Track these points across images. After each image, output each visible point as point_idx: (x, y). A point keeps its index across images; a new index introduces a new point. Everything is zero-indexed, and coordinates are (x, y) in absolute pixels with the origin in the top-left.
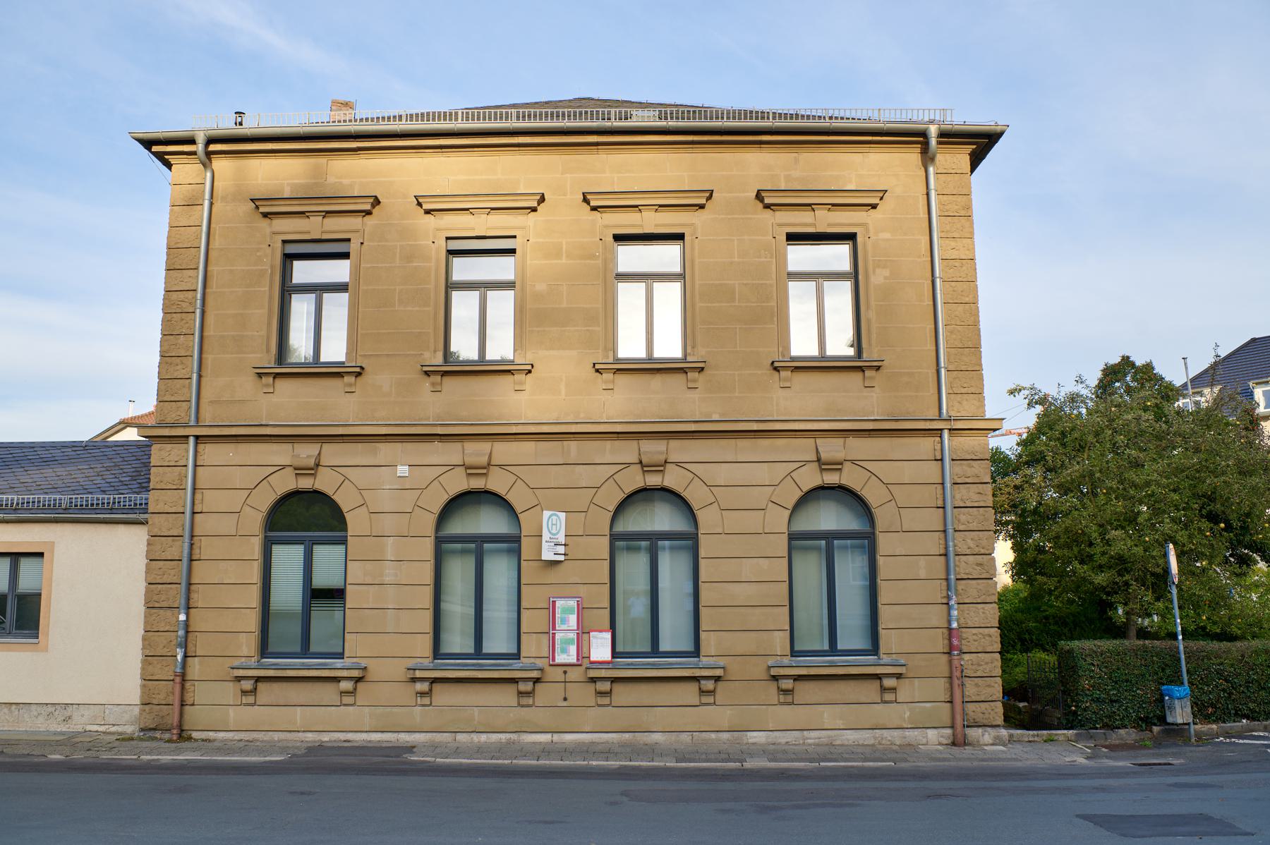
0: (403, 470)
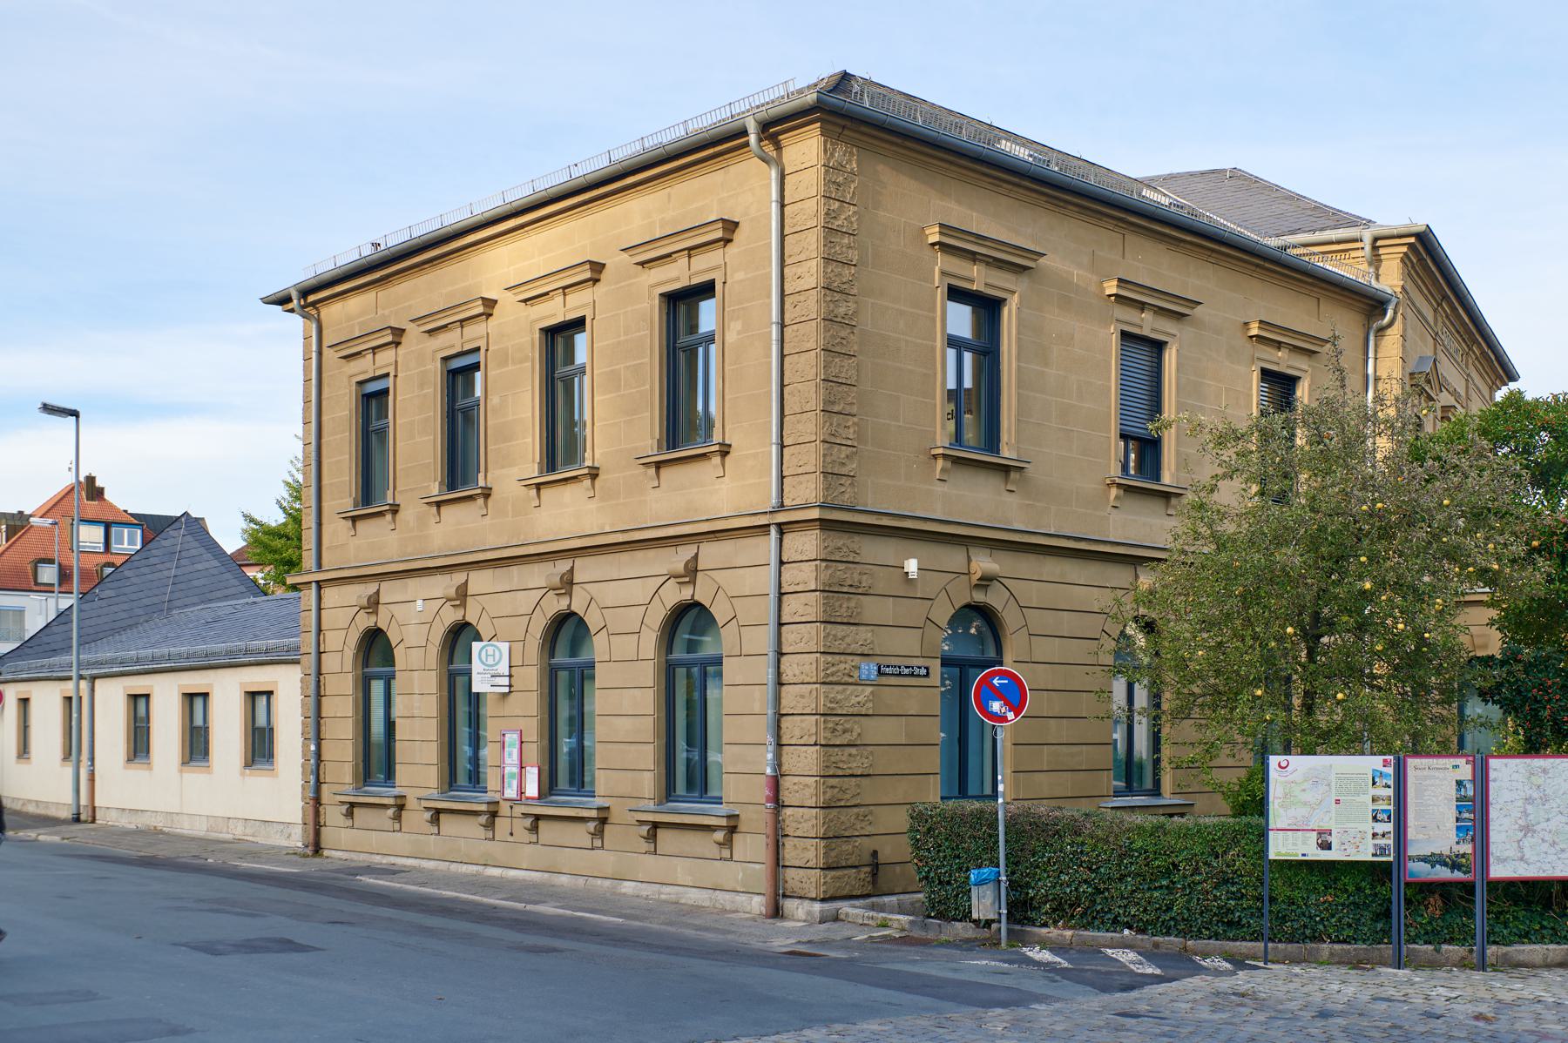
0: (419, 602)
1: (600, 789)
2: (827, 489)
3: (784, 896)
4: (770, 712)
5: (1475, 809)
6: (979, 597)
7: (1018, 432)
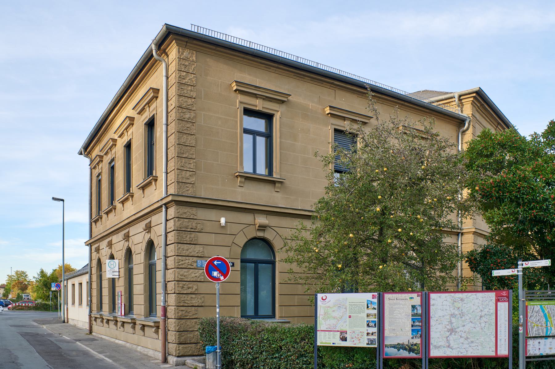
2: (179, 189)
5: (423, 321)
6: (260, 234)
7: (280, 168)
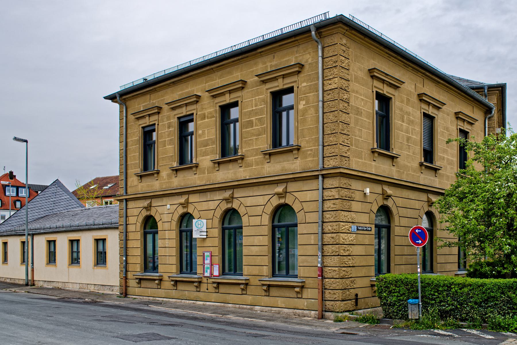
0: (168, 206)
1: (245, 272)
3: (325, 311)
4: (320, 243)
